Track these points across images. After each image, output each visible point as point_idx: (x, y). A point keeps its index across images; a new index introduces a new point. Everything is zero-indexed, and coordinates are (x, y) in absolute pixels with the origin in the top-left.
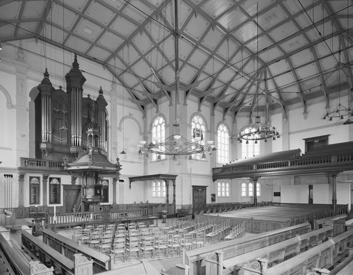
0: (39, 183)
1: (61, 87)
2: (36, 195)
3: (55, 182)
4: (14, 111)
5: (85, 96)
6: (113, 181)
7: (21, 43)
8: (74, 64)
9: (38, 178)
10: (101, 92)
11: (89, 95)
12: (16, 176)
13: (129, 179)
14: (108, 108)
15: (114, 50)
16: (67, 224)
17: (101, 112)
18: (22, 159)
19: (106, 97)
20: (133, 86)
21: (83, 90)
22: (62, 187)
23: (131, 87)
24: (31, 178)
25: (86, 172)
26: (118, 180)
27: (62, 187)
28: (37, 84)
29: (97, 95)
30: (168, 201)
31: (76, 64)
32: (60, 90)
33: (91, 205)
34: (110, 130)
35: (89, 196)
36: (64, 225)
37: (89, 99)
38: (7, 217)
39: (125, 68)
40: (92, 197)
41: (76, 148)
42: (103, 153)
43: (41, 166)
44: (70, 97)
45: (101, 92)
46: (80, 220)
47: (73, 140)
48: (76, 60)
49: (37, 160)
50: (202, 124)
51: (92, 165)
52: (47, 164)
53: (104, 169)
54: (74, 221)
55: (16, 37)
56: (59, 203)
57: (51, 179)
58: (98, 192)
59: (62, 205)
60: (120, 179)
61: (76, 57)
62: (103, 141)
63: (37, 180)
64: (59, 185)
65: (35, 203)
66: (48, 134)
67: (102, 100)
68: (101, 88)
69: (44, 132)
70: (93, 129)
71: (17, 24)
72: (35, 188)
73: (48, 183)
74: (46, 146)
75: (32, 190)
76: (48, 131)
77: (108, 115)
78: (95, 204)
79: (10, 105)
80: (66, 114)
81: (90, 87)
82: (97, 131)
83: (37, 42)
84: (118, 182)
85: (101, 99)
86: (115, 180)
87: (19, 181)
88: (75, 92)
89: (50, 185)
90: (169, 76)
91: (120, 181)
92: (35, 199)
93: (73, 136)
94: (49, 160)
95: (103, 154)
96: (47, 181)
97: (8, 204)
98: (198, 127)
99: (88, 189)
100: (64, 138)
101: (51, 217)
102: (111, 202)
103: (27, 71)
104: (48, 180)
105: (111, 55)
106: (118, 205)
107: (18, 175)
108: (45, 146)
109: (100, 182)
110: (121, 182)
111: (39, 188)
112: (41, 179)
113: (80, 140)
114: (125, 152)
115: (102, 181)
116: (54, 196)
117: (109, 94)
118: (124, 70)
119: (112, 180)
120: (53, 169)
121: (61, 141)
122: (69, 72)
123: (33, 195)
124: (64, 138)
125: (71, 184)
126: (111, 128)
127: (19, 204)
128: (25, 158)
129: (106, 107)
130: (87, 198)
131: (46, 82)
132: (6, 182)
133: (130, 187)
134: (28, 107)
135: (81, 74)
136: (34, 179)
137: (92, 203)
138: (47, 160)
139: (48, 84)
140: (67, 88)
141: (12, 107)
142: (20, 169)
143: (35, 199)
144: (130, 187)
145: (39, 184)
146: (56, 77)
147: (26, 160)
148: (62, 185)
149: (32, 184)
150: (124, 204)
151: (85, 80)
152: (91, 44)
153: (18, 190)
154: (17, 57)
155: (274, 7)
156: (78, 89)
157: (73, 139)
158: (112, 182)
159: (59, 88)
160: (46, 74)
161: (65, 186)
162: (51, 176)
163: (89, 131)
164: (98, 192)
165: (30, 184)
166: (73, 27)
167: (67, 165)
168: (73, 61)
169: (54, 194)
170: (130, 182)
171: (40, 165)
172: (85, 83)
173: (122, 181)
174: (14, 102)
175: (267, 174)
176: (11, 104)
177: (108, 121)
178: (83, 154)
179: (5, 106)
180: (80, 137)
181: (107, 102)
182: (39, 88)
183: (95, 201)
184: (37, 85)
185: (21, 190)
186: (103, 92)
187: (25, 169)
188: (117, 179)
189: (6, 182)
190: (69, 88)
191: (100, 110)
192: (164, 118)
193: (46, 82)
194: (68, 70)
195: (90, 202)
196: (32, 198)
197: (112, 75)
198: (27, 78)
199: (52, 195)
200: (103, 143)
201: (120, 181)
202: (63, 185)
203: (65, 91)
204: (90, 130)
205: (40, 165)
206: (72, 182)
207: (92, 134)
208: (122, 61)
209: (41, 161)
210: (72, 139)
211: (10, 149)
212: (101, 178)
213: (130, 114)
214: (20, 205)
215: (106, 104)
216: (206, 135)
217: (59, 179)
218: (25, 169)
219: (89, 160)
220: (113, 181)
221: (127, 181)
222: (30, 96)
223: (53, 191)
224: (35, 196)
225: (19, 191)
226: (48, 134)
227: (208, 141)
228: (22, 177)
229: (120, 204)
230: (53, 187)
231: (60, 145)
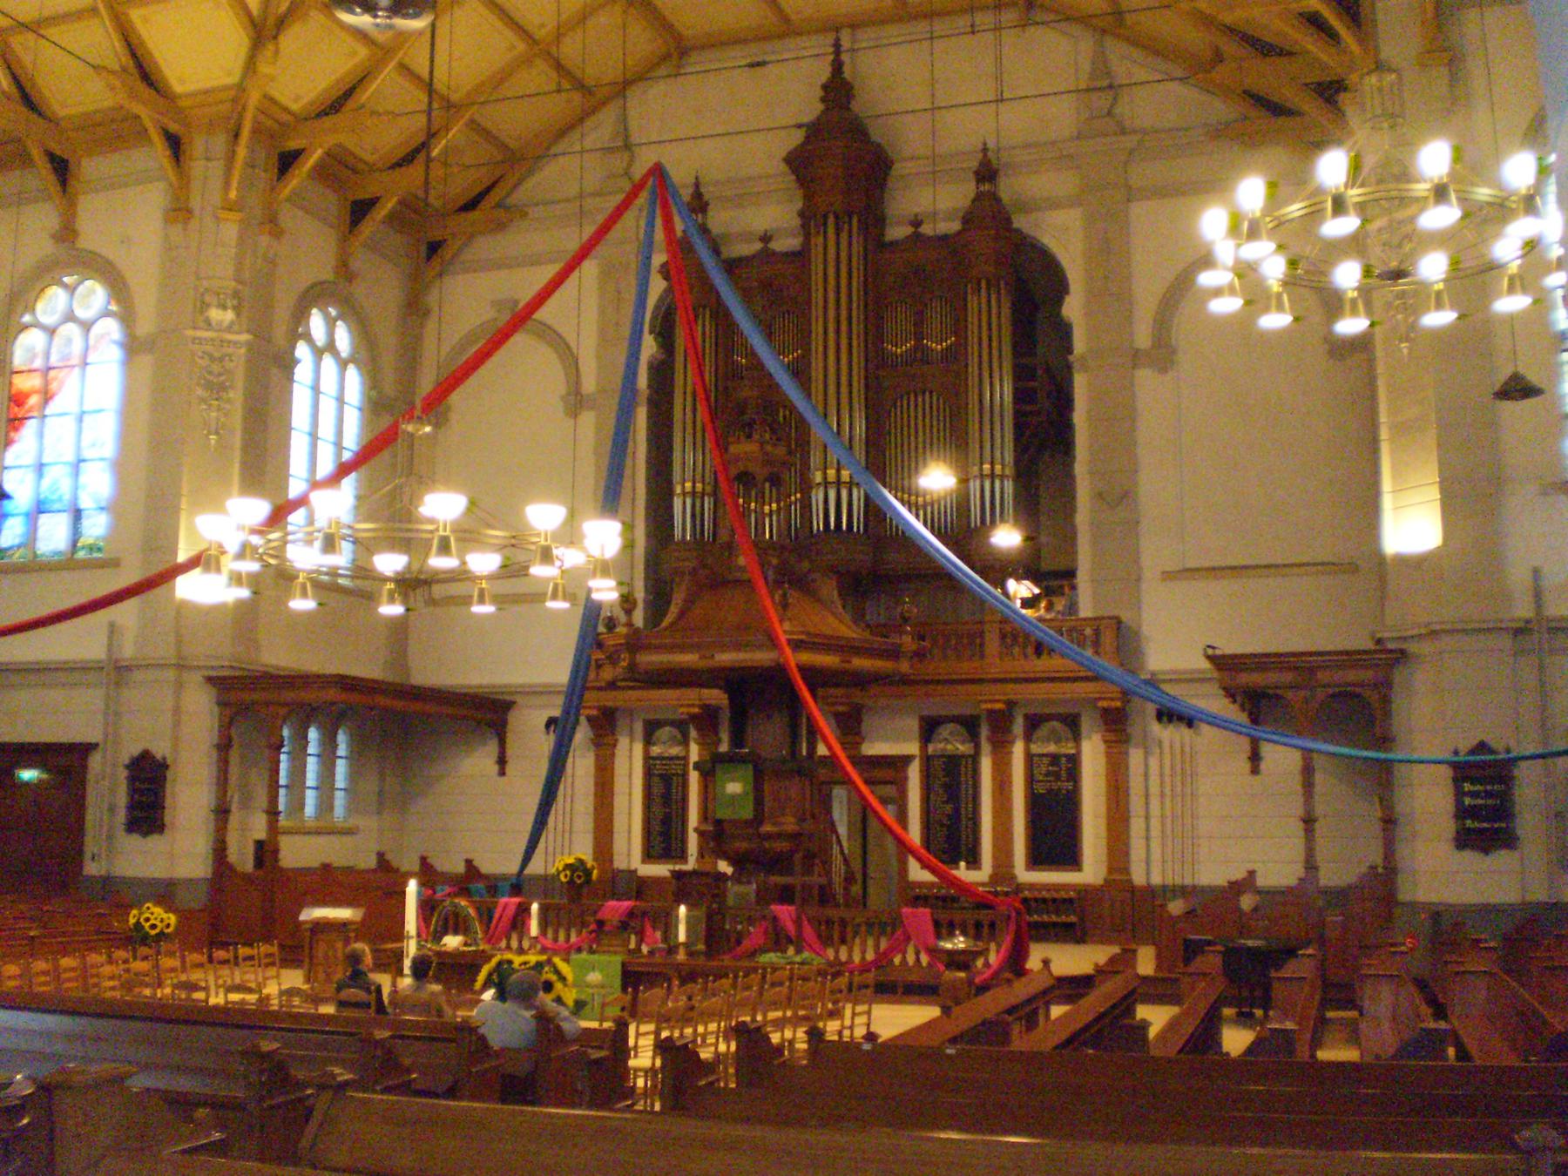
7: (624, 120)
47: (817, 496)
81: (936, 172)
93: (678, 490)
102: (1091, 870)
149: (654, 758)
168: (824, 73)
192: (118, 286)
196: (657, 827)
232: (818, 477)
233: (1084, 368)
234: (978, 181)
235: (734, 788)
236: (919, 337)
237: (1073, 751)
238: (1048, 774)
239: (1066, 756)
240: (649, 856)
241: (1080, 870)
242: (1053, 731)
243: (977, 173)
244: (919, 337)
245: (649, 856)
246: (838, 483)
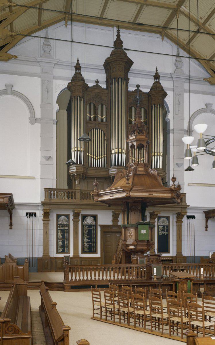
0: (68, 224)
1: (97, 82)
2: (64, 240)
3: (89, 221)
4: (38, 126)
5: (131, 89)
6: (177, 218)
7: (47, 32)
8: (115, 43)
9: (68, 216)
10: (157, 77)
11: (138, 86)
12: (40, 213)
13: (204, 215)
14: (169, 100)
15: (176, 4)
16: (88, 282)
18: (46, 190)
19: (165, 84)
20: (210, 56)
21: (129, 79)
22: (99, 229)
23: (208, 59)
24: (58, 216)
25: (127, 204)
26: (185, 216)
27: (99, 229)
28: (64, 84)
29: (151, 82)
31: (118, 43)
32: (97, 86)
33: (134, 255)
34: (171, 135)
35: (130, 241)
36: (88, 283)
37: (138, 91)
38: (19, 268)
39: (194, 28)
40: (134, 242)
41: (117, 168)
42: (152, 172)
43: (73, 199)
44: (110, 94)
45: (157, 77)
46: (116, 277)
47: (113, 156)
48: (118, 36)
49: (67, 191)
51: (131, 190)
52: (78, 195)
53: (151, 196)
54: (103, 278)
55: (41, 25)
56: (95, 252)
57: (84, 217)
59: (98, 255)
60: (188, 214)
61: (118, 31)
62: (159, 154)
63: (66, 218)
64: (96, 226)
65: (63, 252)
66: (78, 153)
67: (158, 89)
68: (157, 70)
69: (73, 150)
70: (136, 136)
71: (39, 6)
72: (63, 231)
73: (80, 223)
74: (76, 169)
75: (60, 233)
76: (79, 148)
77: (169, 112)
78: (139, 253)
79: (33, 120)
81: (143, 74)
82: (143, 137)
83: (66, 24)
84: (185, 219)
85: (156, 88)
86: (180, 216)
87: (43, 221)
88: (117, 85)
89: (83, 226)
91: (189, 217)
92: (63, 246)
93: (113, 152)
94: (81, 190)
95: (152, 173)
96: (79, 221)
97: (31, 253)
99: (129, 230)
100: (101, 155)
101: (70, 273)
102: (172, 253)
103: (55, 68)
104: (80, 218)
105: (172, 12)
106: (185, 257)
107: (43, 213)
108: (75, 170)
109: (156, 220)
110: (190, 220)
111: (69, 230)
112: (72, 218)
114: (193, 168)
115: (159, 218)
116: (88, 242)
117: (171, 77)
118: (196, 30)
119: (175, 216)
120: (85, 201)
121: (97, 161)
122: (109, 56)
123: (61, 240)
124: (103, 155)
125: (111, 223)
126: (174, 133)
127: (43, 253)
128: (49, 189)
129: (166, 99)
130: (127, 243)
132: (29, 223)
133: (207, 227)
134: (55, 118)
135: (125, 54)
136: (62, 218)
137: (135, 252)
138: (78, 190)
139: (79, 80)
140: (107, 82)
141: (36, 120)
142: (43, 204)
143: (63, 247)
144: (207, 227)
145: (68, 225)
146: (94, 69)
147: (50, 193)
148: (100, 225)
149: (59, 225)
150: (196, 255)
151: (133, 63)
152: (139, 5)
153: (42, 233)
154: (42, 52)
156: (121, 79)
157: (114, 155)
158: (175, 220)
160: (78, 67)
161: (103, 227)
162: (84, 212)
163: (130, 138)
165: (57, 225)
166: (141, 11)
167: (98, 193)
168: (115, 38)
169: (88, 238)
170: (207, 219)
171: (72, 198)
172: (131, 68)
173: (193, 217)
174: (38, 115)
176: (35, 117)
177: (170, 121)
178: (121, 175)
179: (28, 121)
181: (166, 92)
182: (69, 87)
183: (139, 247)
184: (66, 86)
185: (46, 234)
186: (160, 76)
187: (50, 204)
188: (183, 214)
189: (29, 223)
190: (108, 82)
191: (155, 105)
194: (107, 53)
195: (131, 250)
196: (60, 244)
197: (175, 47)
198: (55, 78)
199: (86, 240)
200: (158, 157)
201: (189, 217)
202: (101, 226)
203: (104, 86)
204: (133, 137)
205: (72, 198)
206: (113, 221)
207: (135, 143)
208: (189, 18)
209: (74, 191)
210: (112, 155)
211: (33, 178)
212: (156, 213)
213: (206, 105)
214: (45, 254)
215: (165, 95)
217: (95, 217)
218: (50, 204)
219: (127, 183)
220: (176, 219)
221: (200, 217)
222: (58, 102)
223: (87, 235)
224: (63, 242)
225: (44, 235)
226: (78, 153)
228: (46, 215)
229: (189, 255)
230: (87, 229)
232: (153, 154)
233: (54, 121)
234: (155, 79)
235: (144, 232)
236: (97, 114)
237: (168, 225)
238: (162, 230)
239: (166, 226)
240: (58, 252)
241: (169, 253)
242: (163, 220)
243: (154, 76)
244: (97, 114)
245: (58, 252)
246: (122, 153)
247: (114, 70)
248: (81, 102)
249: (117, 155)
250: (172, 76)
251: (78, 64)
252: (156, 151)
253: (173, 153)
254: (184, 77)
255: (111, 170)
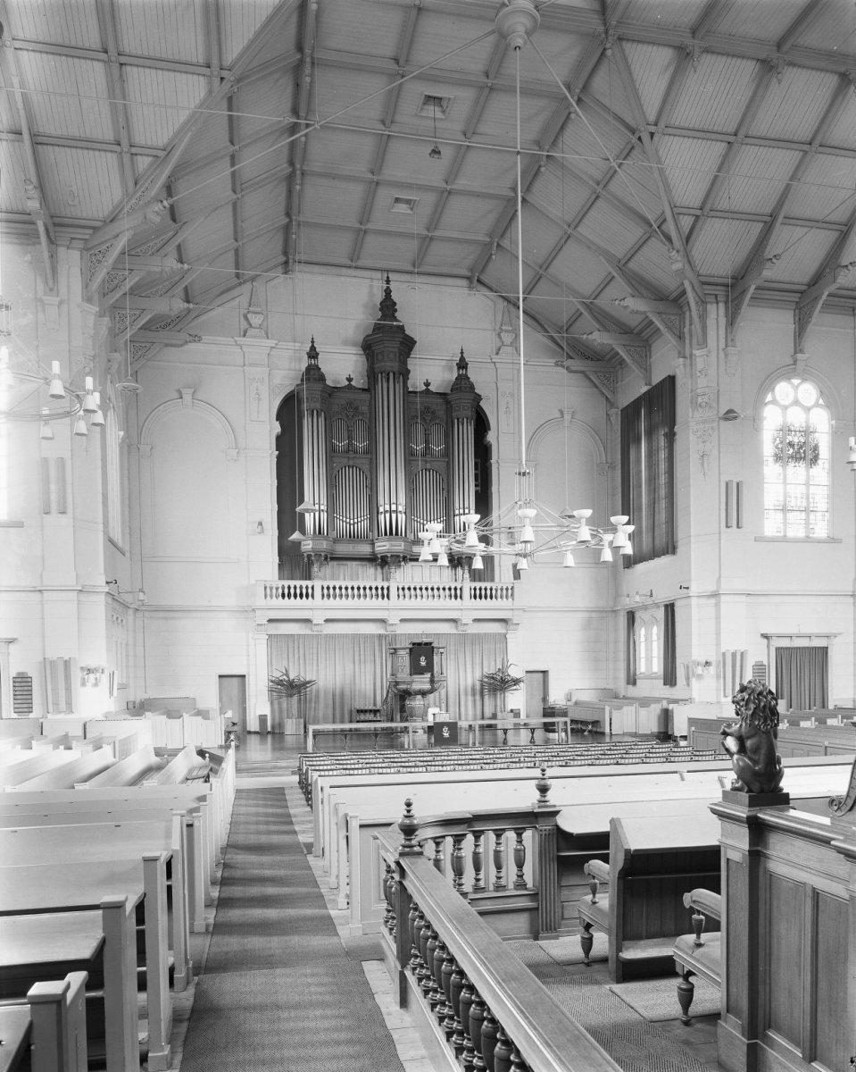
1: (349, 380)
17: (461, 427)
21: (408, 371)
30: (375, 705)
47: (382, 517)
48: (388, 292)
50: (817, 405)
58: (423, 664)
74: (313, 543)
80: (367, 452)
90: (661, 264)
93: (381, 509)
98: (796, 418)
108: (311, 546)
113: (402, 518)
131: (313, 374)
155: (101, 401)
156: (394, 374)
159: (347, 383)
164: (423, 664)
175: (55, 689)
180: (400, 508)
191: (458, 419)
193: (313, 374)
216: (833, 440)
227: (614, 514)
231: (354, 538)
236: (350, 438)
244: (350, 438)
246: (396, 512)
247: (380, 357)
248: (397, 385)
249: (388, 515)
250: (494, 360)
251: (462, 359)
252: (461, 506)
253: (426, 277)
254: (441, 358)
255: (379, 544)
